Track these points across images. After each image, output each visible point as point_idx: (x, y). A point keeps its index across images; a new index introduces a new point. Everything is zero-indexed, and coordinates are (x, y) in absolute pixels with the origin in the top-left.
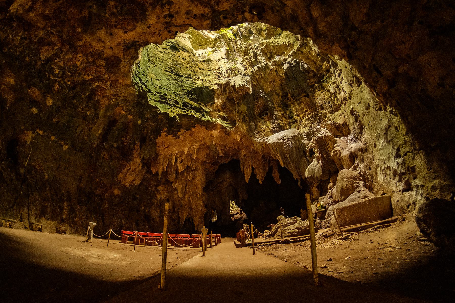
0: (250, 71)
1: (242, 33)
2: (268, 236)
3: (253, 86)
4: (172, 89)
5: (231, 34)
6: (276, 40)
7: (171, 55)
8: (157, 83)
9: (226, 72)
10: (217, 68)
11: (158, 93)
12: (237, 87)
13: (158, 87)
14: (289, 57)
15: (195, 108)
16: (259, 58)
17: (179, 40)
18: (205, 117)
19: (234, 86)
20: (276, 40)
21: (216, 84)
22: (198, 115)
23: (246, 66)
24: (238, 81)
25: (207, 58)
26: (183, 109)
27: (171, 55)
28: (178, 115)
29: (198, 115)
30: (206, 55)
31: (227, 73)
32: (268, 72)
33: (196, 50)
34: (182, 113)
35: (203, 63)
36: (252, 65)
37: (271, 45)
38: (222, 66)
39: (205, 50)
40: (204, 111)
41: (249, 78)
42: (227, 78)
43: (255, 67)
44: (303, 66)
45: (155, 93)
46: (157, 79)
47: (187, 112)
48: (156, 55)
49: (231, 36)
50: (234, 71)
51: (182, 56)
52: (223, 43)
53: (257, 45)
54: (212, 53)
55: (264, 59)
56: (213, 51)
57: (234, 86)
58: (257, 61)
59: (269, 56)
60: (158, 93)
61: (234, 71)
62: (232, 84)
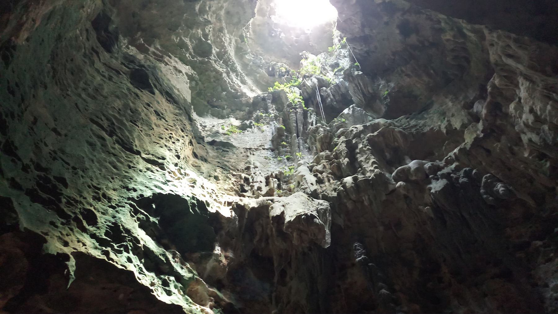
0: (330, 188)
1: (323, 99)
2: (102, 120)
3: (334, 227)
4: (90, 173)
5: (298, 95)
6: (413, 123)
7: (125, 91)
8: (51, 139)
9: (264, 180)
10: (242, 166)
11: (38, 167)
12: (287, 219)
13: (46, 150)
14: (449, 162)
15: (145, 254)
16: (362, 159)
17: (163, 69)
18: (169, 293)
19: (281, 216)
20: (413, 123)
21: (229, 204)
22: (147, 279)
23: (321, 173)
24: (292, 206)
25: (222, 139)
26: (102, 242)
27: (125, 91)
28: (79, 255)
29: (147, 279)
30: (221, 131)
31: (268, 183)
32: (384, 198)
33: (200, 115)
34: (97, 254)
35: (208, 147)
36: (338, 174)
37: (397, 129)
38: (258, 164)
39: (221, 121)
40: (172, 272)
41: (325, 204)
42: (264, 196)
43: (348, 180)
44: (489, 187)
45: (26, 161)
46: (55, 130)
47: (112, 255)
48: (81, 71)
49: (296, 100)
50: (287, 182)
51: (156, 106)
52: (273, 112)
53: (360, 127)
54: (238, 131)
55: (374, 163)
56: (243, 128)
57: (281, 216)
58: (354, 166)
59: (388, 155)
60: (38, 167)
61: (287, 182)
62: (276, 211)
